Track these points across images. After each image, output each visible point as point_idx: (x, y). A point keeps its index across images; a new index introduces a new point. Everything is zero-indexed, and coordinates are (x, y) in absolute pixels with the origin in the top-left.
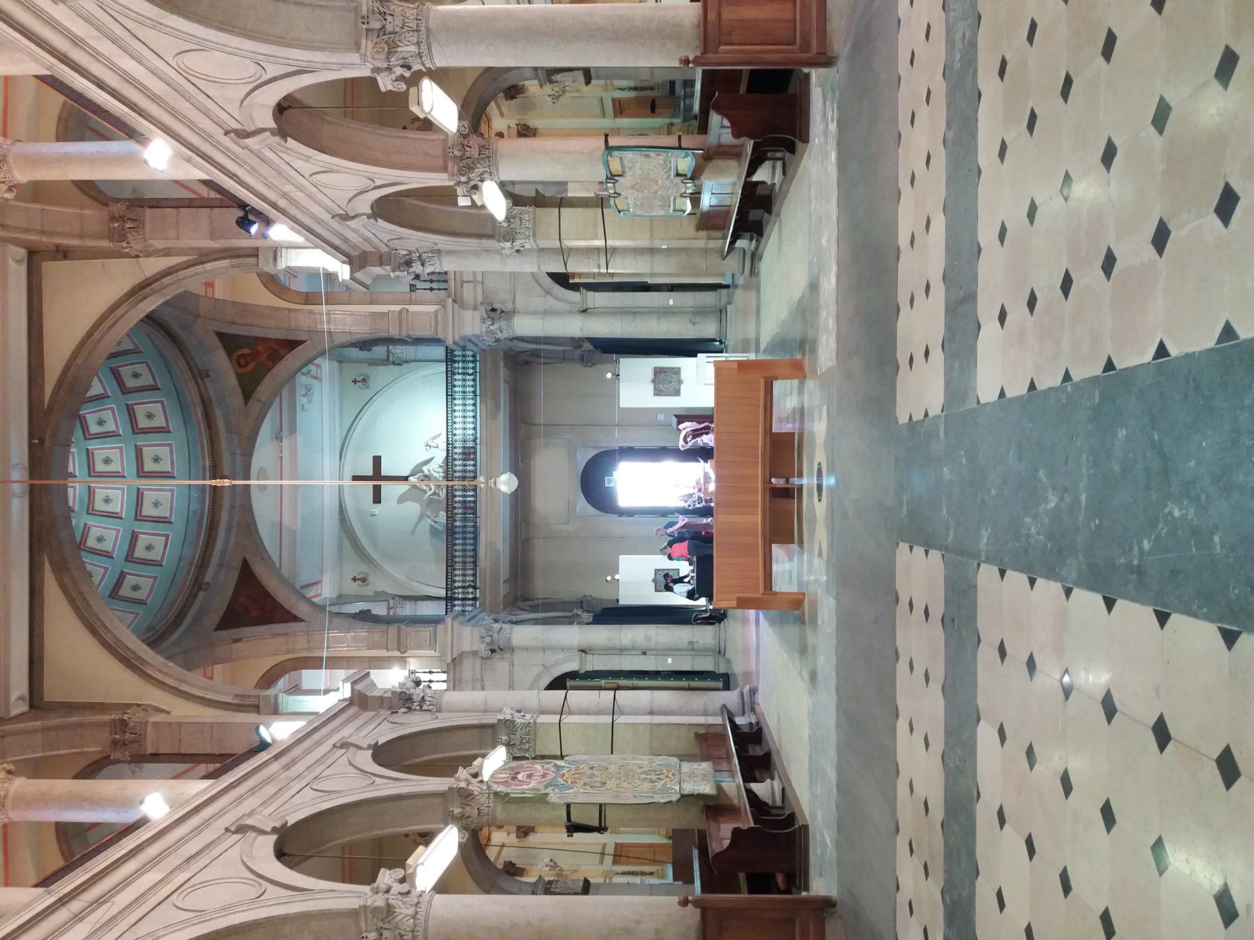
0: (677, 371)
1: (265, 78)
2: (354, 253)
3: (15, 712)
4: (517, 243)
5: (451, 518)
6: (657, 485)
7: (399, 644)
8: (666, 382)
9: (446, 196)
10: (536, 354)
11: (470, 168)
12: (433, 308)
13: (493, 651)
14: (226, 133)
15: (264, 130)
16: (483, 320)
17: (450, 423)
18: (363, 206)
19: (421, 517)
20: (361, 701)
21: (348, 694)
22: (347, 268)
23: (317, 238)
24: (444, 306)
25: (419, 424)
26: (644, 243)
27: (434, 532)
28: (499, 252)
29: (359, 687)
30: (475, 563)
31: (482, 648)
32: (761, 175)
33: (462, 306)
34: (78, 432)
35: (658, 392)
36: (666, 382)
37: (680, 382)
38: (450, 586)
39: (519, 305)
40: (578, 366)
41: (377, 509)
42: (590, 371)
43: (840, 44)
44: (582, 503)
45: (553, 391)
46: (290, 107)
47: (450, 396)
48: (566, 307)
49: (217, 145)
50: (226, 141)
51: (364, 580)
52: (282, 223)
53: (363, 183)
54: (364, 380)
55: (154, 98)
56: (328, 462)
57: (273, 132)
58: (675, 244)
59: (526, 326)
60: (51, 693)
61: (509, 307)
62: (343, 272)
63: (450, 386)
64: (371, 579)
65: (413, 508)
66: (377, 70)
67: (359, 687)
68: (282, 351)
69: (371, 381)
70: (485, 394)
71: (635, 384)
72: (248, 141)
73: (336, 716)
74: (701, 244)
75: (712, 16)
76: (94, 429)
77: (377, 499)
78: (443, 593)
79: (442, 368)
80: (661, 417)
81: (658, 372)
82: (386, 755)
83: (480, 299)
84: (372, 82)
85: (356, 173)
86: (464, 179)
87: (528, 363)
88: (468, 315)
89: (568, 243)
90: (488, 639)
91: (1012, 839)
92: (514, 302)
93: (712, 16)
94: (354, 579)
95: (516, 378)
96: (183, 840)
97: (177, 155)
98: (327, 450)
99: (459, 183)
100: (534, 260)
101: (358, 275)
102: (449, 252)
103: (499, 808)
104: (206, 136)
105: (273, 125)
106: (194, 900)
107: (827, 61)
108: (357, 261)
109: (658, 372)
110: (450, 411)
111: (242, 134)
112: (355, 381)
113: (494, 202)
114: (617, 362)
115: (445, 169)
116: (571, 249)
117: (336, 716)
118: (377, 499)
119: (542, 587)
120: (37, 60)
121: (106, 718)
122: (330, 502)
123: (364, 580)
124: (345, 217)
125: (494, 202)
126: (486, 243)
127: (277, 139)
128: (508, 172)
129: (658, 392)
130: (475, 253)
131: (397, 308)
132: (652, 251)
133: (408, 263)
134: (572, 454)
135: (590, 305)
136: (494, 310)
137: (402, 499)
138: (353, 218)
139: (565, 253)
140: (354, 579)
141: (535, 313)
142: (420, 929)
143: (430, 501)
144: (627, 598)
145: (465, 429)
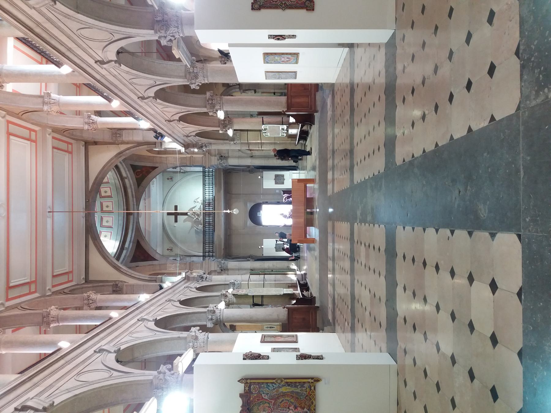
0: (283, 176)
1: (114, 39)
2: (186, 144)
3: (47, 294)
4: (235, 142)
5: (204, 227)
6: (276, 215)
7: (190, 268)
8: (279, 180)
9: (206, 114)
10: (233, 169)
11: (226, 126)
12: (202, 156)
13: (222, 270)
14: (96, 62)
15: (112, 61)
16: (218, 160)
17: (204, 193)
18: (151, 93)
19: (192, 227)
20: (187, 279)
21: (184, 276)
22: (184, 148)
23: (176, 140)
24: (205, 155)
25: (192, 194)
26: (273, 142)
27: (197, 232)
28: (230, 144)
29: (187, 274)
30: (213, 242)
31: (218, 270)
32: (305, 128)
33: (211, 155)
34: (98, 196)
35: (276, 183)
36: (279, 180)
37: (284, 179)
38: (204, 252)
39: (230, 155)
40: (248, 173)
41: (176, 224)
42: (252, 175)
43: (319, 108)
44: (249, 222)
45: (240, 184)
46: (122, 52)
47: (204, 184)
48: (246, 155)
49: (93, 69)
50: (95, 66)
51: (171, 250)
52: (67, 64)
53: (152, 82)
54: (171, 178)
55: (151, 115)
56: (159, 207)
57: (116, 62)
58: (281, 142)
59: (232, 162)
60: (91, 278)
61: (227, 155)
62: (183, 150)
63: (204, 181)
64: (173, 249)
65: (189, 224)
66: (160, 37)
67: (187, 274)
68: (151, 170)
69: (174, 179)
70: (217, 184)
71: (268, 181)
72: (105, 66)
73: (180, 282)
74: (289, 142)
75: (289, 101)
76: (103, 194)
77: (176, 221)
78: (202, 254)
79: (39, 94)
80: (277, 191)
81: (276, 176)
82: (200, 289)
83: (217, 153)
84: (158, 42)
85: (174, 108)
86: (193, 82)
87: (230, 172)
88: (213, 158)
89: (249, 141)
90: (220, 266)
91: (360, 305)
92: (228, 153)
93: (289, 101)
94: (168, 250)
95: (228, 179)
96: (147, 308)
97: (121, 104)
98: (158, 204)
99: (192, 84)
100: (240, 146)
101: (187, 150)
102: (214, 144)
103: (234, 299)
104: (160, 121)
105: (115, 59)
106: (83, 378)
107: (317, 112)
108: (187, 146)
109: (276, 176)
110: (204, 189)
111: (102, 62)
112: (168, 179)
113: (230, 132)
114: (262, 172)
115: (206, 107)
116: (250, 143)
117: (180, 282)
118: (176, 221)
119: (235, 251)
120: (19, 30)
121: (112, 284)
122: (159, 221)
123: (171, 250)
124: (143, 98)
125: (230, 132)
126: (225, 141)
127: (117, 65)
128: (236, 127)
129: (276, 183)
130: (222, 144)
131: (189, 156)
132: (275, 143)
133: (202, 147)
134: (246, 205)
135: (254, 155)
136: (222, 156)
137: (185, 221)
138: (147, 98)
139: (249, 144)
140: (168, 250)
141: (235, 157)
142: (221, 313)
143: (195, 222)
144: (266, 254)
145: (209, 196)
